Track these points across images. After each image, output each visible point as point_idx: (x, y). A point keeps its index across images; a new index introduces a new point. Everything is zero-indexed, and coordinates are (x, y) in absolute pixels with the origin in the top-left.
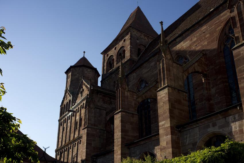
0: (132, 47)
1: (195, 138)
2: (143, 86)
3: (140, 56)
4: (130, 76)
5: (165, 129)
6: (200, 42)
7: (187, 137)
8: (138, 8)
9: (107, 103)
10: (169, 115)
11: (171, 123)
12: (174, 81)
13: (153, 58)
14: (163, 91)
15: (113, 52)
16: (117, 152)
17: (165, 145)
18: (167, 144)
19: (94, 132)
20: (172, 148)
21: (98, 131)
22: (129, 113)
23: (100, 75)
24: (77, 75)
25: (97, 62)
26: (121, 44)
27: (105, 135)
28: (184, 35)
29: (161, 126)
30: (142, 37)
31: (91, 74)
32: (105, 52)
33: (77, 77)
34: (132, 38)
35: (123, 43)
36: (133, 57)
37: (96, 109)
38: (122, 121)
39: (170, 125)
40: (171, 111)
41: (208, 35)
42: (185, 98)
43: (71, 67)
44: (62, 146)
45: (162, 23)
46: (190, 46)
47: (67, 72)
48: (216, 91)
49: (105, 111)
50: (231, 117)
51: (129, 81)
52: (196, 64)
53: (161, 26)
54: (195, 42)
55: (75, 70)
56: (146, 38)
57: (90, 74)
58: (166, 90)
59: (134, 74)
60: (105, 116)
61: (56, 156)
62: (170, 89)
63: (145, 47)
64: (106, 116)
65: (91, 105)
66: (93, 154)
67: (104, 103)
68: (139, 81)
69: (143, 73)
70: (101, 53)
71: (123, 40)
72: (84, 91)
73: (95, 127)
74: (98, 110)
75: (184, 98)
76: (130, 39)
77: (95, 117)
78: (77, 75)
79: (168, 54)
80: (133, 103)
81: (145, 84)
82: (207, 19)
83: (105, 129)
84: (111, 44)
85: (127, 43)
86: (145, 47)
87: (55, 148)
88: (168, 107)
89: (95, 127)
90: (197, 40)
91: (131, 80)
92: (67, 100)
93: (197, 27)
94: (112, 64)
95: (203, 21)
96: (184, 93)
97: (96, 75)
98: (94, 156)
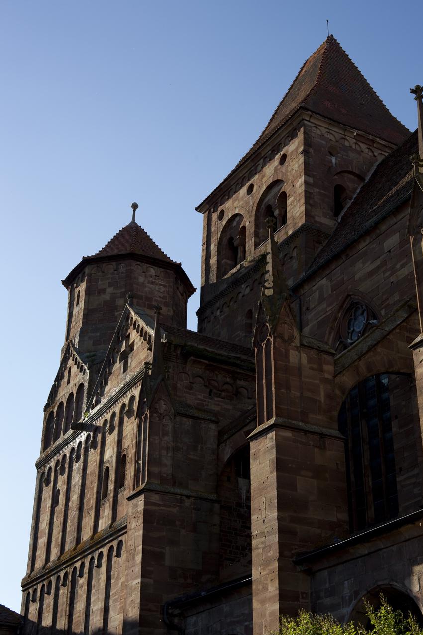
0: (311, 180)
3: (342, 214)
4: (306, 288)
15: (241, 204)
21: (187, 502)
25: (184, 243)
26: (270, 171)
27: (217, 520)
30: (347, 144)
32: (211, 204)
33: (107, 297)
34: (311, 150)
35: (276, 169)
36: (317, 219)
37: (178, 419)
43: (86, 262)
44: (50, 564)
47: (70, 282)
49: (213, 426)
51: (304, 309)
56: (364, 147)
57: (157, 288)
60: (215, 446)
61: (26, 605)
63: (361, 178)
67: (210, 395)
68: (342, 307)
69: (357, 277)
70: (196, 209)
74: (187, 423)
78: (110, 290)
80: (322, 394)
83: (213, 496)
86: (361, 178)
87: (22, 571)
89: (178, 490)
91: (312, 306)
92: (72, 384)
97: (181, 288)
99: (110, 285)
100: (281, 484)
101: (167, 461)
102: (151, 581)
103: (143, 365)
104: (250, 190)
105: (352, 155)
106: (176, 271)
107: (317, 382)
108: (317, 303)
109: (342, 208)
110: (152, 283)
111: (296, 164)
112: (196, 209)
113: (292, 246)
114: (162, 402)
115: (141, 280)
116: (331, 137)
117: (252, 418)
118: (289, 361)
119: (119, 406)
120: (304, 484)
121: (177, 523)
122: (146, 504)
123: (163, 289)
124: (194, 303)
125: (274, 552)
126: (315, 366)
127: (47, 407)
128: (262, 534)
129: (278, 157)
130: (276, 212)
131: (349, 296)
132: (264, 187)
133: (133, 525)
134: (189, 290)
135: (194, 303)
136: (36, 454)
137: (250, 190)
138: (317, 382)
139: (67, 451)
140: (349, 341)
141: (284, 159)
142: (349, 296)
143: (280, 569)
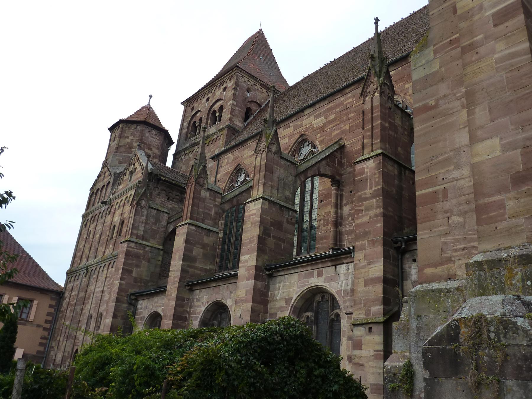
0: (235, 103)
1: (291, 290)
2: (242, 178)
3: (248, 122)
4: (222, 156)
5: (248, 269)
6: (339, 123)
7: (280, 287)
8: (261, 31)
9: (175, 200)
10: (256, 246)
11: (257, 260)
12: (278, 190)
13: (311, 110)
14: (255, 205)
15: (203, 106)
16: (171, 295)
17: (244, 296)
18: (246, 295)
19: (141, 252)
20: (253, 301)
21: (148, 248)
22: (202, 228)
23: (173, 143)
24: (131, 137)
25: (172, 121)
26: (218, 93)
27: (160, 258)
28: (317, 106)
29: (243, 263)
30: (256, 87)
31: (154, 139)
32: (188, 103)
33: (128, 141)
34: (238, 88)
35: (221, 93)
36: (235, 122)
37: (150, 209)
38: (187, 241)
39: (256, 263)
40: (261, 241)
41: (351, 115)
42: (291, 219)
43: (121, 121)
44: (81, 266)
45: (377, 20)
46: (324, 126)
47: (111, 129)
48: (351, 212)
49: (166, 215)
50: (343, 266)
51: (219, 165)
52: (324, 162)
53: (374, 26)
54: (331, 122)
55: (127, 128)
56: (264, 90)
57: (155, 140)
58: (260, 202)
59: (230, 155)
60: (166, 224)
61: (66, 283)
62: (267, 203)
63: (260, 105)
64: (167, 224)
65: (143, 201)
66: (131, 291)
67: (168, 199)
68: (235, 168)
69: (244, 157)
70: (181, 103)
71: (222, 87)
72: (135, 171)
73: (144, 243)
74: (154, 212)
75: (290, 220)
76: (235, 89)
77: (146, 224)
78: (131, 137)
79: (274, 143)
80: (213, 211)
81: (245, 177)
82: (353, 87)
83: (161, 247)
84: (203, 88)
85: (226, 95)
86: (260, 105)
87: (68, 268)
88: (257, 233)
89: (144, 243)
90: (335, 120)
91: (223, 165)
92: (105, 180)
93: (339, 96)
94: (196, 127)
95: (349, 89)
96: (291, 212)
97: (167, 142)
98: (132, 294)
99: (131, 135)
100: (186, 249)
101: (142, 228)
102: (124, 282)
103: (137, 181)
104: (208, 100)
105: (258, 93)
106: (165, 134)
107: (212, 206)
108: (225, 164)
109: (248, 118)
110: (153, 137)
111: (230, 93)
112: (181, 103)
113: (221, 133)
114: (143, 201)
115: (147, 135)
116: (249, 83)
117: (180, 218)
118: (200, 195)
119: (125, 197)
120: (197, 251)
121: (141, 257)
122: (128, 247)
123: (157, 141)
124: (172, 150)
125: (177, 279)
126: (212, 198)
127: (92, 189)
128: (174, 270)
129: (222, 87)
130: (217, 114)
131: (239, 164)
132: (214, 101)
133: (120, 256)
134: (170, 142)
135: (172, 150)
136: (83, 211)
137: (208, 100)
138: (212, 206)
139: (97, 212)
140: (236, 185)
141: (225, 89)
142: (239, 164)
143: (179, 287)
